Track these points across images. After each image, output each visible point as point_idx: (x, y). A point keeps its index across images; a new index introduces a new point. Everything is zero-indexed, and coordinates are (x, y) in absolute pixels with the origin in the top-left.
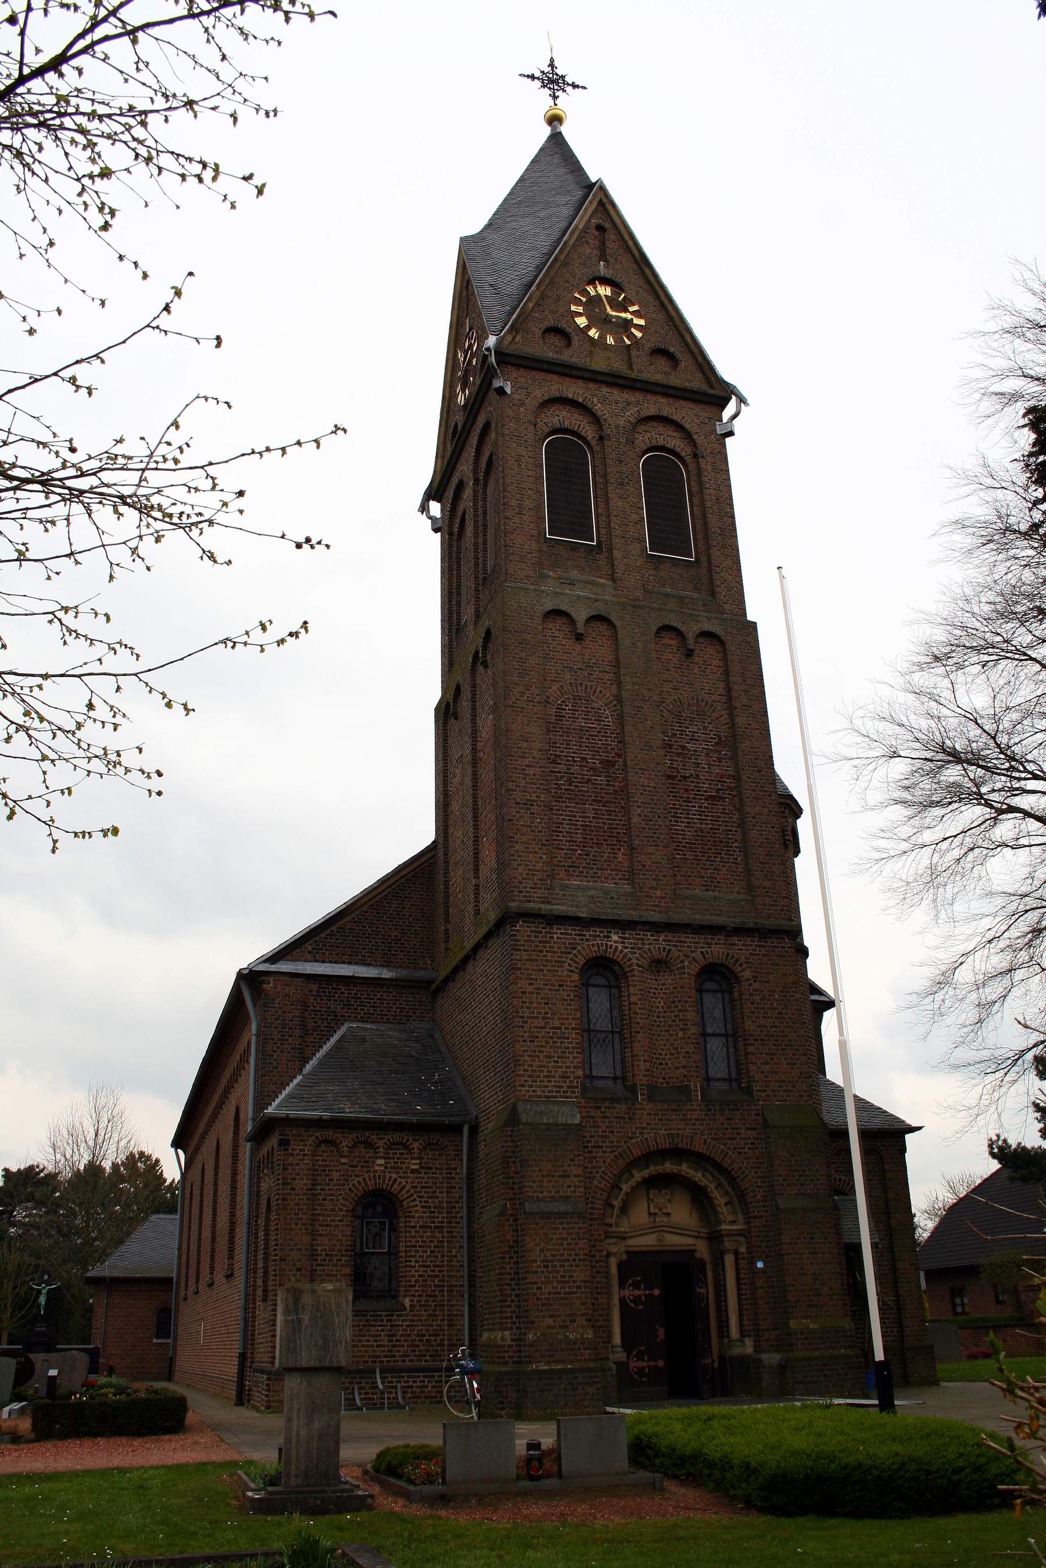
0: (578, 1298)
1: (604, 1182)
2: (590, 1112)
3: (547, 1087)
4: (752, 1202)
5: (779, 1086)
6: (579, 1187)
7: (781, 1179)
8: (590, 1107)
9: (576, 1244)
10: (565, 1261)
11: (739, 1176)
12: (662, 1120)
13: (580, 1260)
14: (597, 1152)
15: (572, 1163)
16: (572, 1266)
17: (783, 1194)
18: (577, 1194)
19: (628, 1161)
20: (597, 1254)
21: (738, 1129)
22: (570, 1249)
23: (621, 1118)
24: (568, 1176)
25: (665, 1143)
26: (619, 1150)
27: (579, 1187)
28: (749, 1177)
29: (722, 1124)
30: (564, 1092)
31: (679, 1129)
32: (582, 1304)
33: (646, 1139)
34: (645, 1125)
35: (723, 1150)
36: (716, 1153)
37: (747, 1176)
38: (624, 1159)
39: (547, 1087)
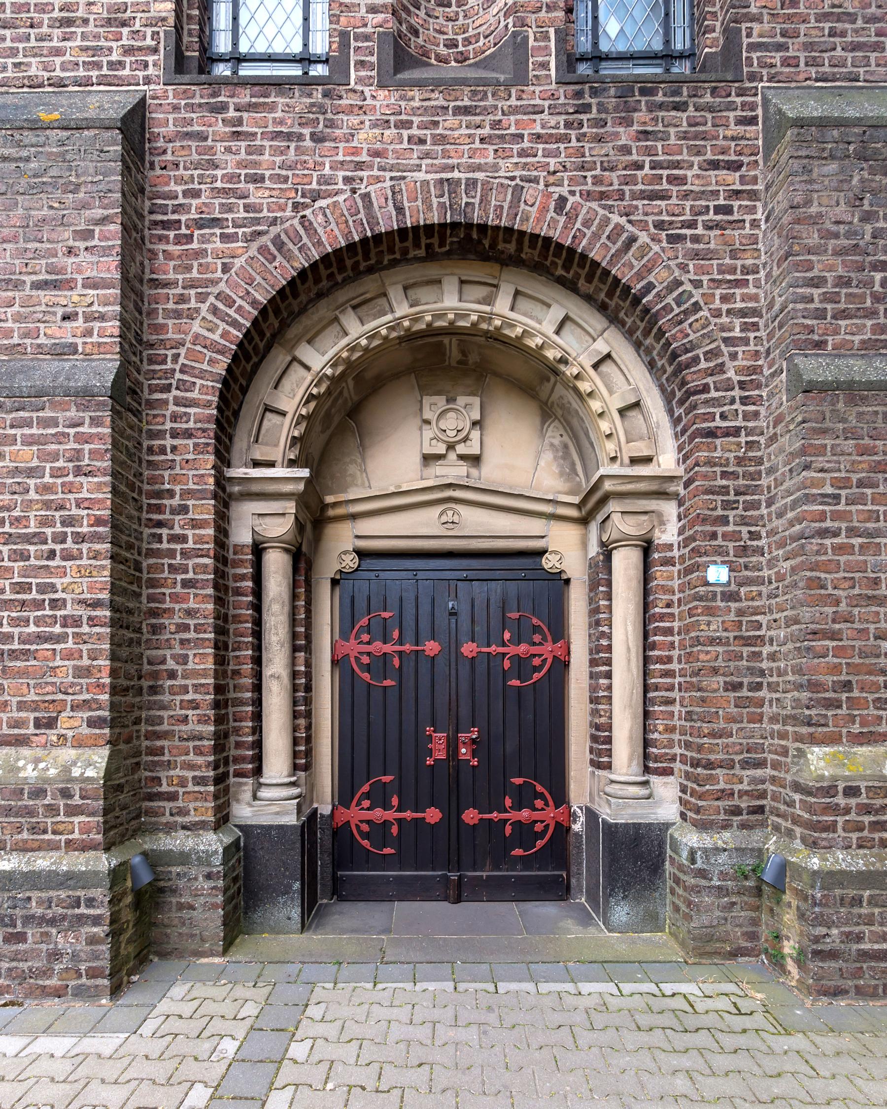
0: (68, 655)
1: (222, 326)
2: (190, 122)
3: (58, 52)
4: (705, 389)
5: (833, 33)
6: (102, 317)
7: (816, 292)
8: (191, 107)
9: (69, 488)
10: (29, 539)
11: (667, 309)
12: (422, 141)
13: (80, 538)
14: (204, 240)
15: (82, 245)
16: (52, 555)
17: (820, 345)
18: (95, 339)
19: (302, 262)
20: (190, 533)
21: (677, 165)
22: (47, 505)
23: (289, 137)
24: (68, 285)
25: (430, 208)
26: (274, 230)
27: (102, 317)
28: (704, 313)
29: (626, 150)
30: (112, 65)
31: (479, 168)
32: (82, 672)
33: (366, 197)
34: (364, 157)
35: (619, 229)
36: (596, 236)
37: (696, 307)
38: (288, 257)
39: (58, 52)
